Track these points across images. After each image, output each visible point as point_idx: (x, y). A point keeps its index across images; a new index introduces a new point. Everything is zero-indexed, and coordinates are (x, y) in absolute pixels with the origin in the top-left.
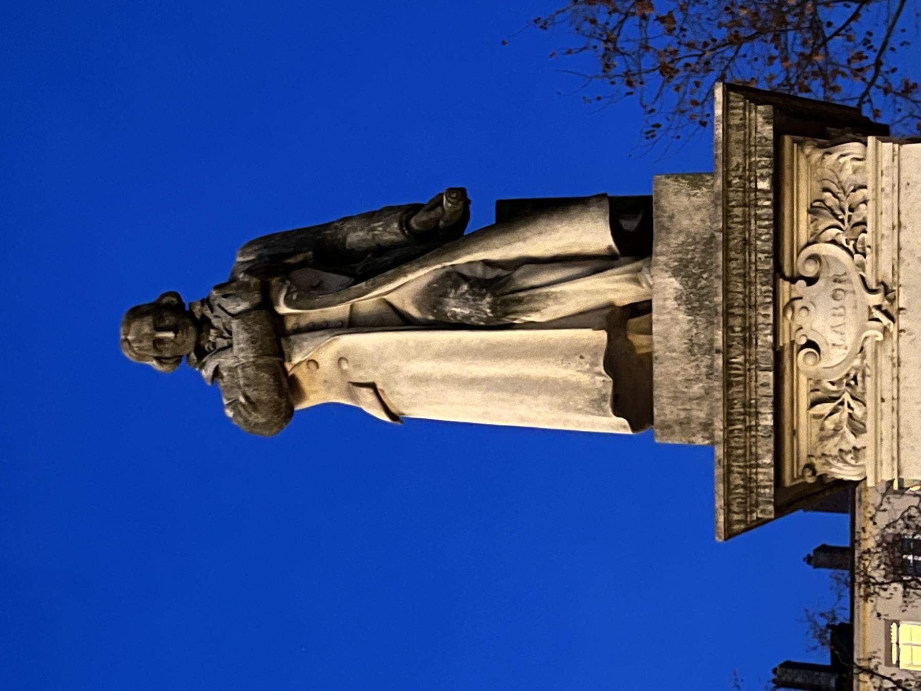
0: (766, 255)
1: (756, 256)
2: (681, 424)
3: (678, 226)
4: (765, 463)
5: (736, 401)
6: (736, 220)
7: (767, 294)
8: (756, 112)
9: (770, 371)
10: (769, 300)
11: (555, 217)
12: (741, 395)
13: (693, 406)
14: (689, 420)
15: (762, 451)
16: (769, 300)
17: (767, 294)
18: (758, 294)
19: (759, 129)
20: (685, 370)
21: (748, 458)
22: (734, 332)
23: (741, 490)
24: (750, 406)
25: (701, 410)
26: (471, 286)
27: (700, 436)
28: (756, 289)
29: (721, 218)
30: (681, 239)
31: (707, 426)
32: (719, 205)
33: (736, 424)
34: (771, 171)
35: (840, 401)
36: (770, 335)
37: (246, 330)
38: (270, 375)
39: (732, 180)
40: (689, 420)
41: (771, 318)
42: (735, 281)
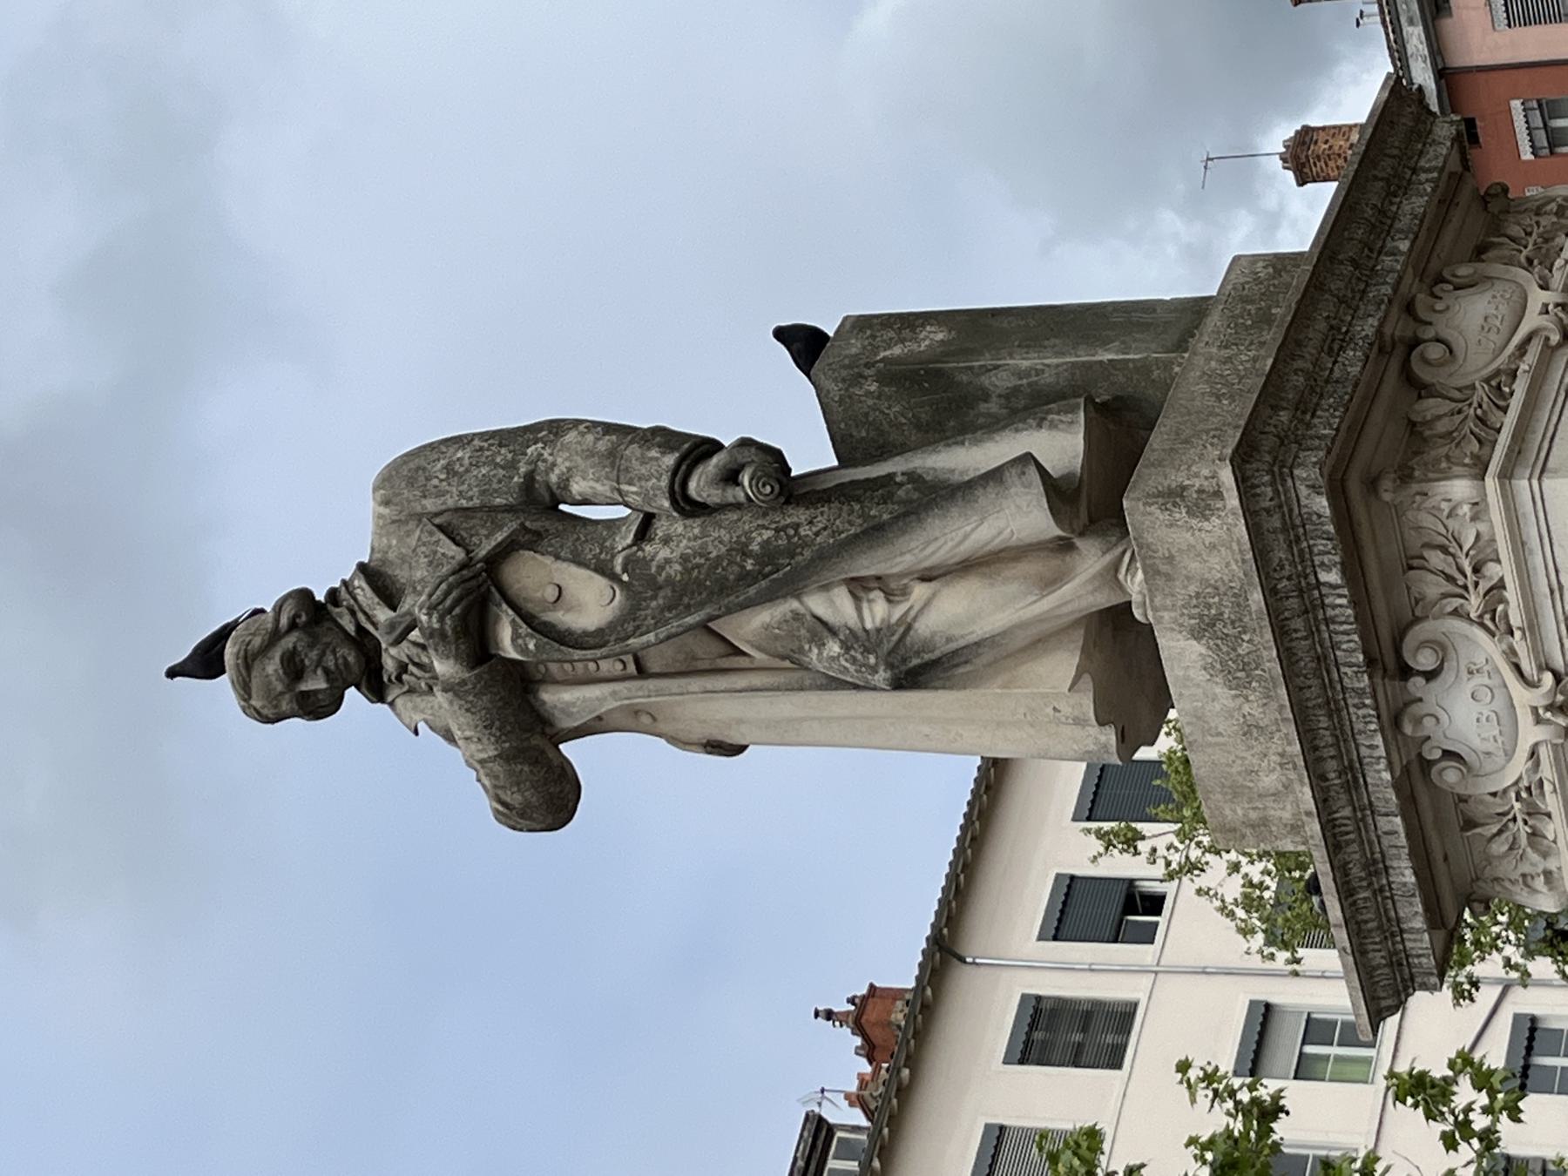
0: (1355, 669)
1: (1338, 670)
2: (1253, 826)
3: (1184, 572)
4: (1413, 928)
5: (1351, 866)
6: (1299, 635)
7: (1368, 719)
8: (1293, 478)
9: (1396, 816)
10: (1373, 727)
11: (955, 511)
12: (1357, 856)
13: (1267, 804)
14: (1265, 822)
15: (1357, 658)
16: (1373, 727)
17: (1368, 719)
18: (1354, 719)
19: (1304, 502)
20: (1243, 758)
21: (1386, 927)
22: (1327, 780)
23: (1386, 970)
24: (1375, 862)
25: (1283, 809)
26: (847, 648)
27: (1289, 840)
28: (1349, 713)
29: (1272, 643)
30: (1192, 589)
31: (1295, 829)
32: (1265, 626)
33: (1358, 893)
34: (1337, 559)
35: (1510, 816)
36: (1385, 770)
37: (468, 710)
38: (530, 764)
39: (1276, 585)
40: (1265, 822)
41: (1382, 748)
42: (1315, 715)
